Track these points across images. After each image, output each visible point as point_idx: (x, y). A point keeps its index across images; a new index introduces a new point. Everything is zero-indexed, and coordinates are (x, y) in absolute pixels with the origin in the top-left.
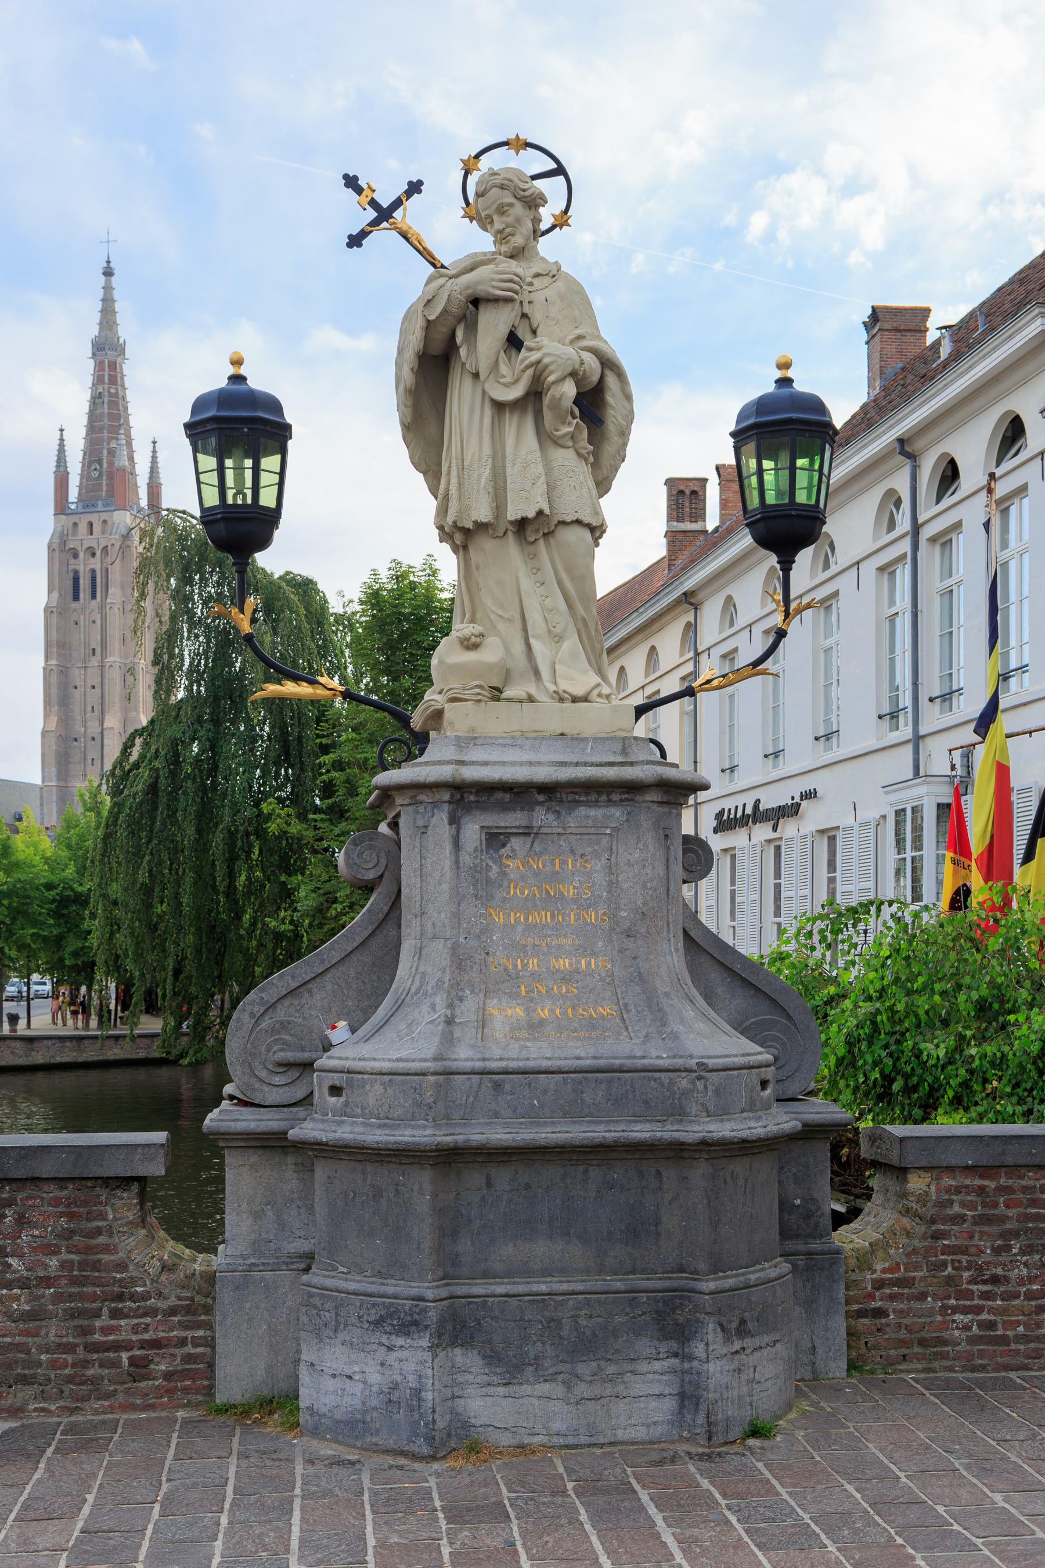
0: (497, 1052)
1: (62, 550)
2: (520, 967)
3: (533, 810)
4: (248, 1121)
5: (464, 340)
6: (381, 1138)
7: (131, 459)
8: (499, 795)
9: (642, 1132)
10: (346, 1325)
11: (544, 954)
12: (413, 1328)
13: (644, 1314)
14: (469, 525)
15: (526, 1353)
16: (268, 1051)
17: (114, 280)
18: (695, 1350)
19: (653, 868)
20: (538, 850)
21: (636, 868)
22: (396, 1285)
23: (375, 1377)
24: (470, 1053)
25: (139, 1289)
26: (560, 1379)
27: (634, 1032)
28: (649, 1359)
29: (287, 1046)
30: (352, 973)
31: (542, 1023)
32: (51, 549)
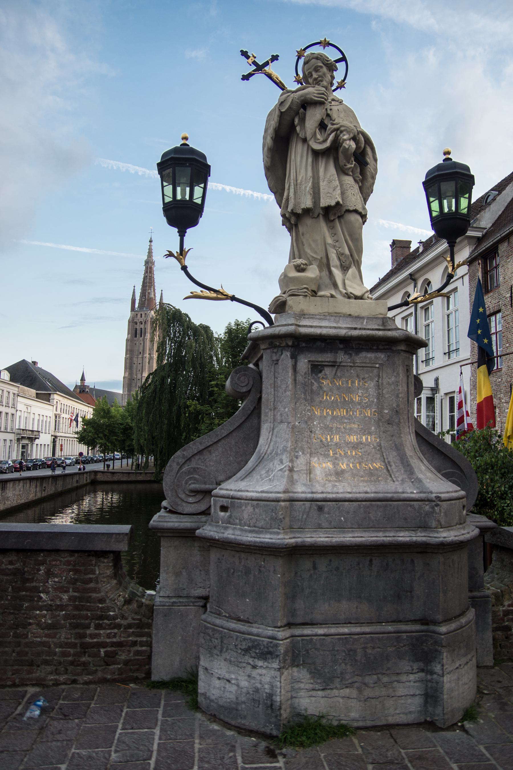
0: (319, 489)
1: (132, 322)
2: (329, 440)
3: (337, 353)
4: (173, 522)
5: (298, 124)
6: (252, 539)
7: (155, 295)
8: (319, 344)
9: (404, 537)
10: (227, 649)
11: (342, 433)
12: (269, 656)
13: (405, 646)
14: (300, 211)
15: (336, 670)
16: (186, 483)
17: (152, 244)
18: (435, 668)
19: (402, 386)
20: (339, 375)
21: (392, 386)
22: (258, 628)
23: (244, 683)
24: (303, 489)
25: (111, 613)
26: (355, 686)
27: (395, 477)
28: (408, 673)
29: (197, 481)
30: (233, 442)
31: (343, 472)
32: (129, 322)
